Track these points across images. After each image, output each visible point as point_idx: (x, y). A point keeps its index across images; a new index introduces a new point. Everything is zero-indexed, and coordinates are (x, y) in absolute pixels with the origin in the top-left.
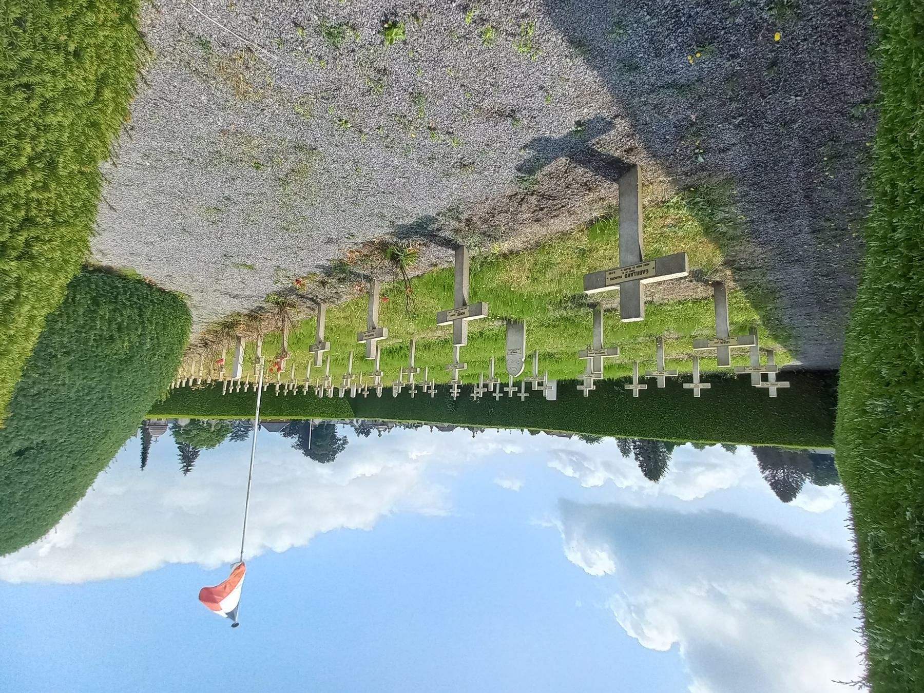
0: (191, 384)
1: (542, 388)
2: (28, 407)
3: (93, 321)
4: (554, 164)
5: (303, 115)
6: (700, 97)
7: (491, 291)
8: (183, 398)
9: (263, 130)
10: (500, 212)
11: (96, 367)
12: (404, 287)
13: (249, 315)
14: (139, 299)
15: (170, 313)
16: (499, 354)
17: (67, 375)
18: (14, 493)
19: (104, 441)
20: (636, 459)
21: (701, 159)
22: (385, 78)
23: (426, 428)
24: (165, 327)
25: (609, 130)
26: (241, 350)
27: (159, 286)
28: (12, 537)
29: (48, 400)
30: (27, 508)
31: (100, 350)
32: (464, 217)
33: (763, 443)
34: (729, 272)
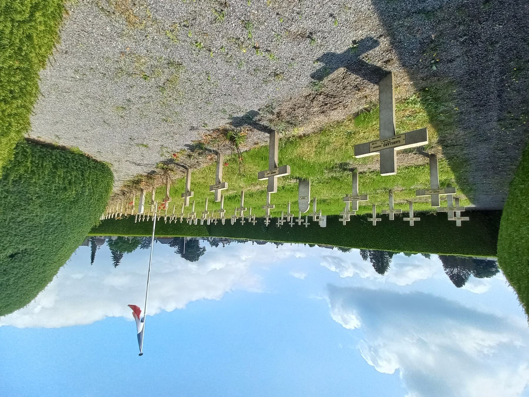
0: (116, 216)
1: (318, 220)
2: (16, 229)
3: (54, 178)
4: (336, 73)
5: (172, 40)
6: (439, 21)
7: (291, 160)
8: (110, 225)
9: (148, 51)
10: (299, 108)
11: (56, 206)
12: (237, 159)
13: (147, 176)
14: (81, 166)
15: (100, 174)
16: (294, 200)
17: (39, 210)
18: (9, 279)
19: (62, 249)
20: (371, 261)
21: (434, 68)
22: (226, 9)
23: (250, 243)
24: (97, 182)
25: (375, 47)
26: (144, 197)
27: (94, 158)
28: (8, 305)
29: (28, 224)
30: (17, 288)
31: (58, 195)
32: (276, 111)
33: (451, 253)
34: (440, 148)
